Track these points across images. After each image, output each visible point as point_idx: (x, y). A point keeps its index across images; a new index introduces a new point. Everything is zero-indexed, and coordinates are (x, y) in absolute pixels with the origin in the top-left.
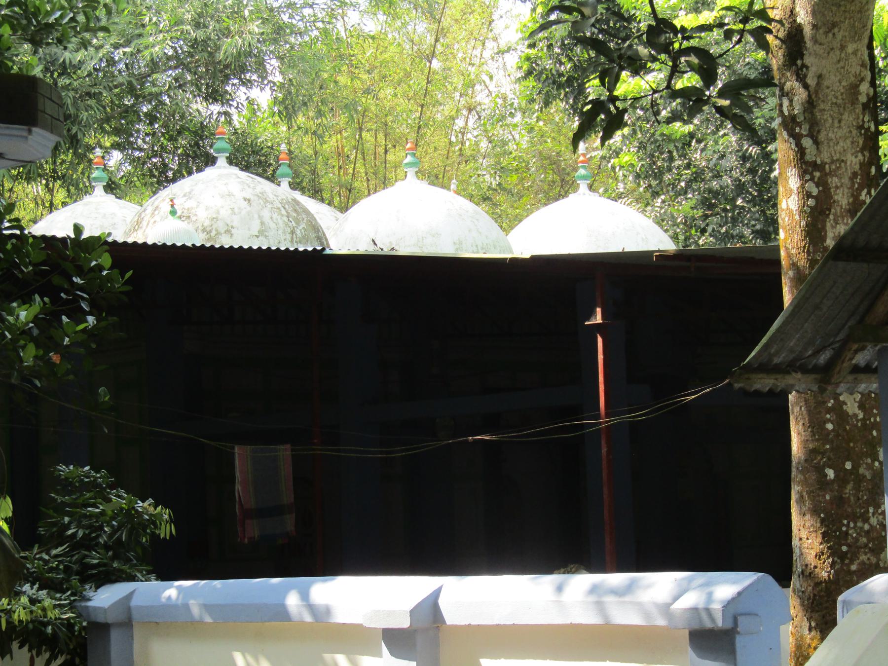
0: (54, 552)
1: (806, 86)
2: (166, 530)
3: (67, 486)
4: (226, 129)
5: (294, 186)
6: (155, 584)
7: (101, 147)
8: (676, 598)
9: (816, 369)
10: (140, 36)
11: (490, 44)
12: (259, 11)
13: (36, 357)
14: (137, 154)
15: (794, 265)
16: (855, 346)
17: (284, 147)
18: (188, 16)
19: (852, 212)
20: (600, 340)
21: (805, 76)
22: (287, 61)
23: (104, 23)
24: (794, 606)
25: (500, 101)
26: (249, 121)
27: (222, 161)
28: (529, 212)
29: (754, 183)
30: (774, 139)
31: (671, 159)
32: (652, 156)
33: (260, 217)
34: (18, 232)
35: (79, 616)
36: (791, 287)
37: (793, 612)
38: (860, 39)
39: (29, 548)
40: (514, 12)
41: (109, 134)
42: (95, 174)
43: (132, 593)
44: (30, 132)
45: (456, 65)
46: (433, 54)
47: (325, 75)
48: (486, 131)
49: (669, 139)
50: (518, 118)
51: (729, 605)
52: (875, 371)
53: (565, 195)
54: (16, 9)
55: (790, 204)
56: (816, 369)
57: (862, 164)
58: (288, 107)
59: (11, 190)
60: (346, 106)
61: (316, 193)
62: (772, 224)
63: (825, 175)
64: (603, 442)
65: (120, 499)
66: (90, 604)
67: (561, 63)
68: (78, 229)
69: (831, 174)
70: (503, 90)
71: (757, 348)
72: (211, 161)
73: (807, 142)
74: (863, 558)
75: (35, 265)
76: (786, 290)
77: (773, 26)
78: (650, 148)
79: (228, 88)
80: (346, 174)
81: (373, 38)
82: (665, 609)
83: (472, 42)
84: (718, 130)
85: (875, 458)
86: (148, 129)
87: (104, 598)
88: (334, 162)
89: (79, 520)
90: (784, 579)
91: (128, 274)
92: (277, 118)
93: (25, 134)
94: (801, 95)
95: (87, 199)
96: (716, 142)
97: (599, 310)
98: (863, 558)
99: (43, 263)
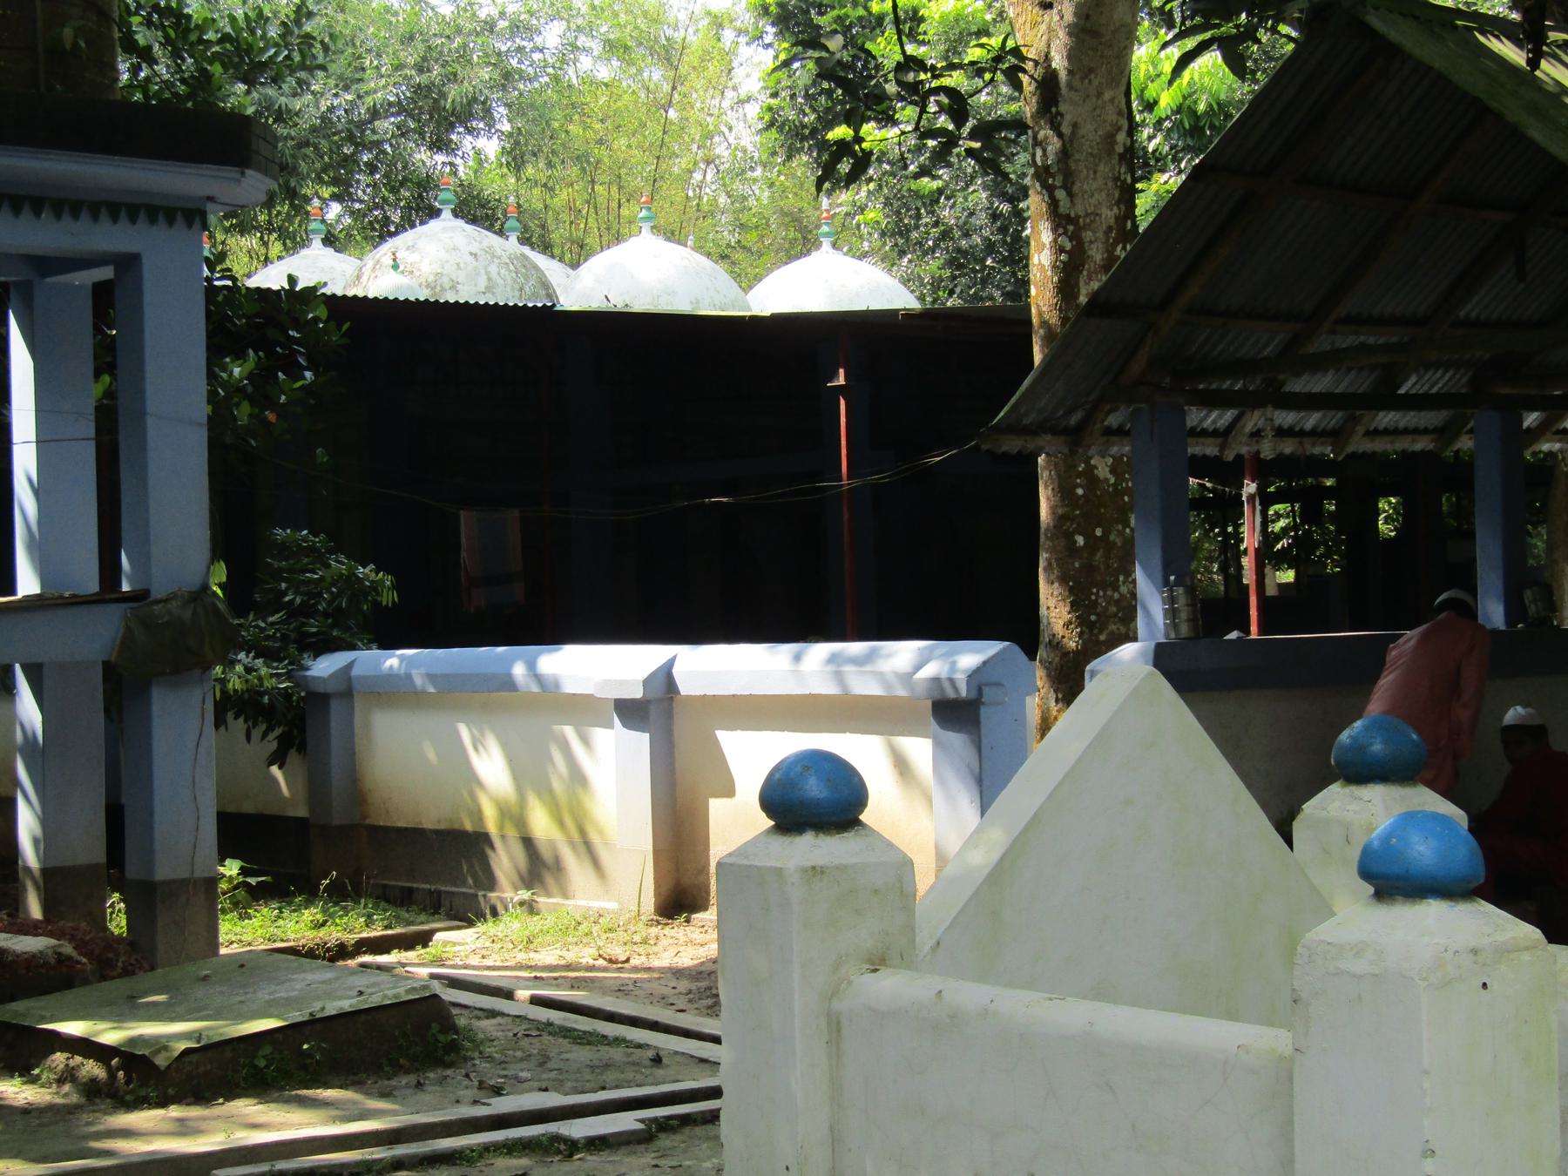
0: (271, 619)
1: (1060, 135)
2: (389, 597)
3: (284, 550)
4: (452, 180)
5: (524, 241)
6: (375, 653)
7: (319, 198)
8: (918, 668)
9: (1066, 431)
10: (361, 80)
11: (730, 94)
12: (487, 55)
13: (250, 416)
14: (357, 206)
15: (1044, 324)
16: (1108, 407)
17: (512, 199)
18: (411, 61)
19: (1106, 268)
20: (842, 402)
21: (1060, 125)
22: (517, 109)
23: (320, 60)
24: (1040, 676)
25: (740, 155)
26: (476, 172)
27: (447, 214)
28: (769, 271)
29: (1005, 242)
30: (1026, 196)
31: (918, 217)
32: (898, 213)
33: (487, 273)
34: (229, 283)
35: (297, 685)
36: (1042, 346)
37: (1039, 683)
38: (1117, 86)
39: (243, 615)
40: (756, 60)
41: (328, 184)
42: (313, 226)
43: (352, 663)
44: (243, 174)
45: (694, 115)
46: (670, 104)
47: (556, 125)
48: (724, 185)
49: (917, 194)
50: (758, 172)
51: (974, 674)
52: (1127, 433)
53: (809, 252)
54: (228, 46)
55: (1042, 259)
56: (1066, 431)
57: (1117, 218)
58: (516, 158)
59: (223, 243)
60: (578, 158)
61: (546, 248)
62: (1022, 286)
63: (1079, 229)
64: (845, 509)
65: (339, 565)
66: (309, 673)
67: (805, 115)
68: (292, 280)
69: (1086, 227)
70: (743, 143)
71: (1006, 409)
72: (434, 213)
73: (1060, 194)
74: (1113, 627)
75: (248, 317)
76: (1036, 349)
77: (1029, 66)
78: (896, 204)
79: (454, 137)
80: (577, 229)
81: (606, 85)
82: (906, 678)
83: (711, 91)
84: (967, 186)
85: (1127, 524)
86: (369, 180)
87: (324, 667)
88: (565, 217)
89: (296, 586)
90: (1031, 652)
91: (345, 327)
92: (505, 170)
93: (238, 176)
94: (1054, 144)
95: (304, 252)
96: (966, 199)
97: (841, 371)
98: (1113, 627)
99: (257, 315)
